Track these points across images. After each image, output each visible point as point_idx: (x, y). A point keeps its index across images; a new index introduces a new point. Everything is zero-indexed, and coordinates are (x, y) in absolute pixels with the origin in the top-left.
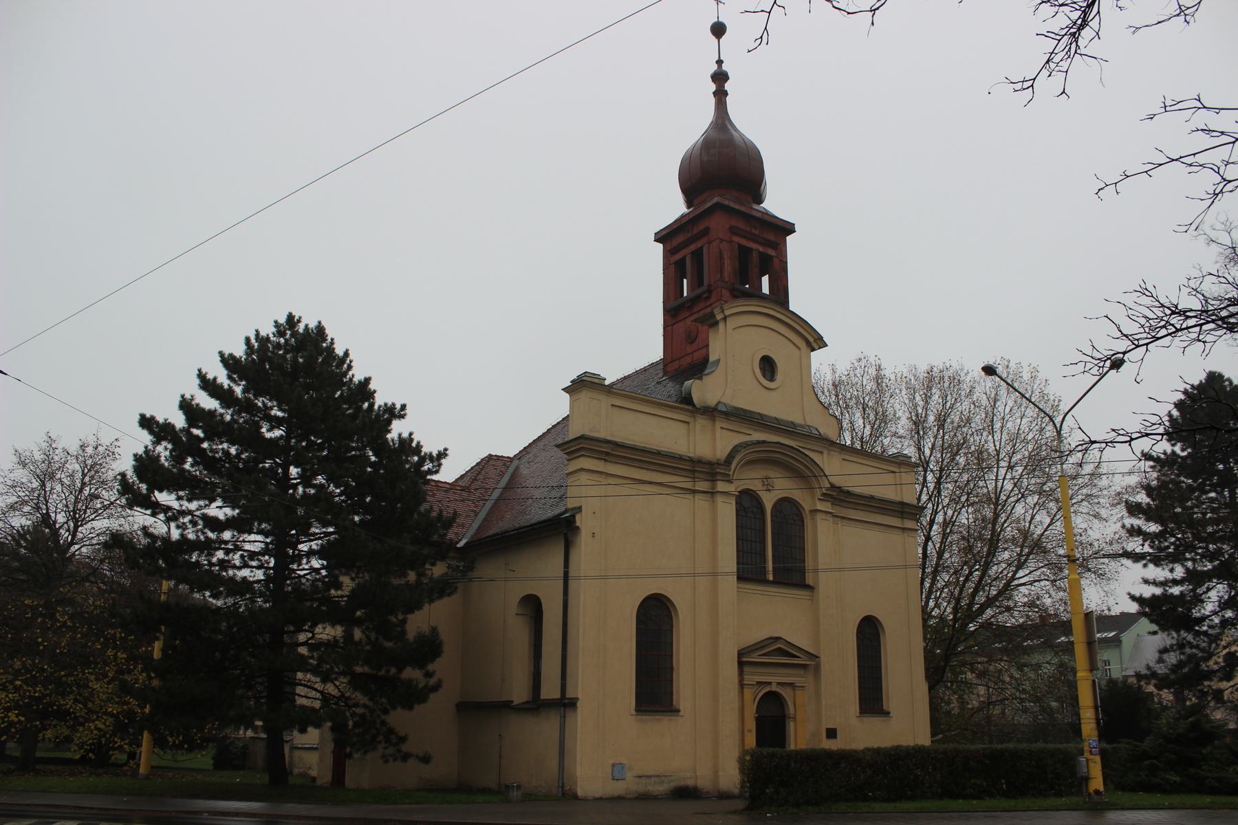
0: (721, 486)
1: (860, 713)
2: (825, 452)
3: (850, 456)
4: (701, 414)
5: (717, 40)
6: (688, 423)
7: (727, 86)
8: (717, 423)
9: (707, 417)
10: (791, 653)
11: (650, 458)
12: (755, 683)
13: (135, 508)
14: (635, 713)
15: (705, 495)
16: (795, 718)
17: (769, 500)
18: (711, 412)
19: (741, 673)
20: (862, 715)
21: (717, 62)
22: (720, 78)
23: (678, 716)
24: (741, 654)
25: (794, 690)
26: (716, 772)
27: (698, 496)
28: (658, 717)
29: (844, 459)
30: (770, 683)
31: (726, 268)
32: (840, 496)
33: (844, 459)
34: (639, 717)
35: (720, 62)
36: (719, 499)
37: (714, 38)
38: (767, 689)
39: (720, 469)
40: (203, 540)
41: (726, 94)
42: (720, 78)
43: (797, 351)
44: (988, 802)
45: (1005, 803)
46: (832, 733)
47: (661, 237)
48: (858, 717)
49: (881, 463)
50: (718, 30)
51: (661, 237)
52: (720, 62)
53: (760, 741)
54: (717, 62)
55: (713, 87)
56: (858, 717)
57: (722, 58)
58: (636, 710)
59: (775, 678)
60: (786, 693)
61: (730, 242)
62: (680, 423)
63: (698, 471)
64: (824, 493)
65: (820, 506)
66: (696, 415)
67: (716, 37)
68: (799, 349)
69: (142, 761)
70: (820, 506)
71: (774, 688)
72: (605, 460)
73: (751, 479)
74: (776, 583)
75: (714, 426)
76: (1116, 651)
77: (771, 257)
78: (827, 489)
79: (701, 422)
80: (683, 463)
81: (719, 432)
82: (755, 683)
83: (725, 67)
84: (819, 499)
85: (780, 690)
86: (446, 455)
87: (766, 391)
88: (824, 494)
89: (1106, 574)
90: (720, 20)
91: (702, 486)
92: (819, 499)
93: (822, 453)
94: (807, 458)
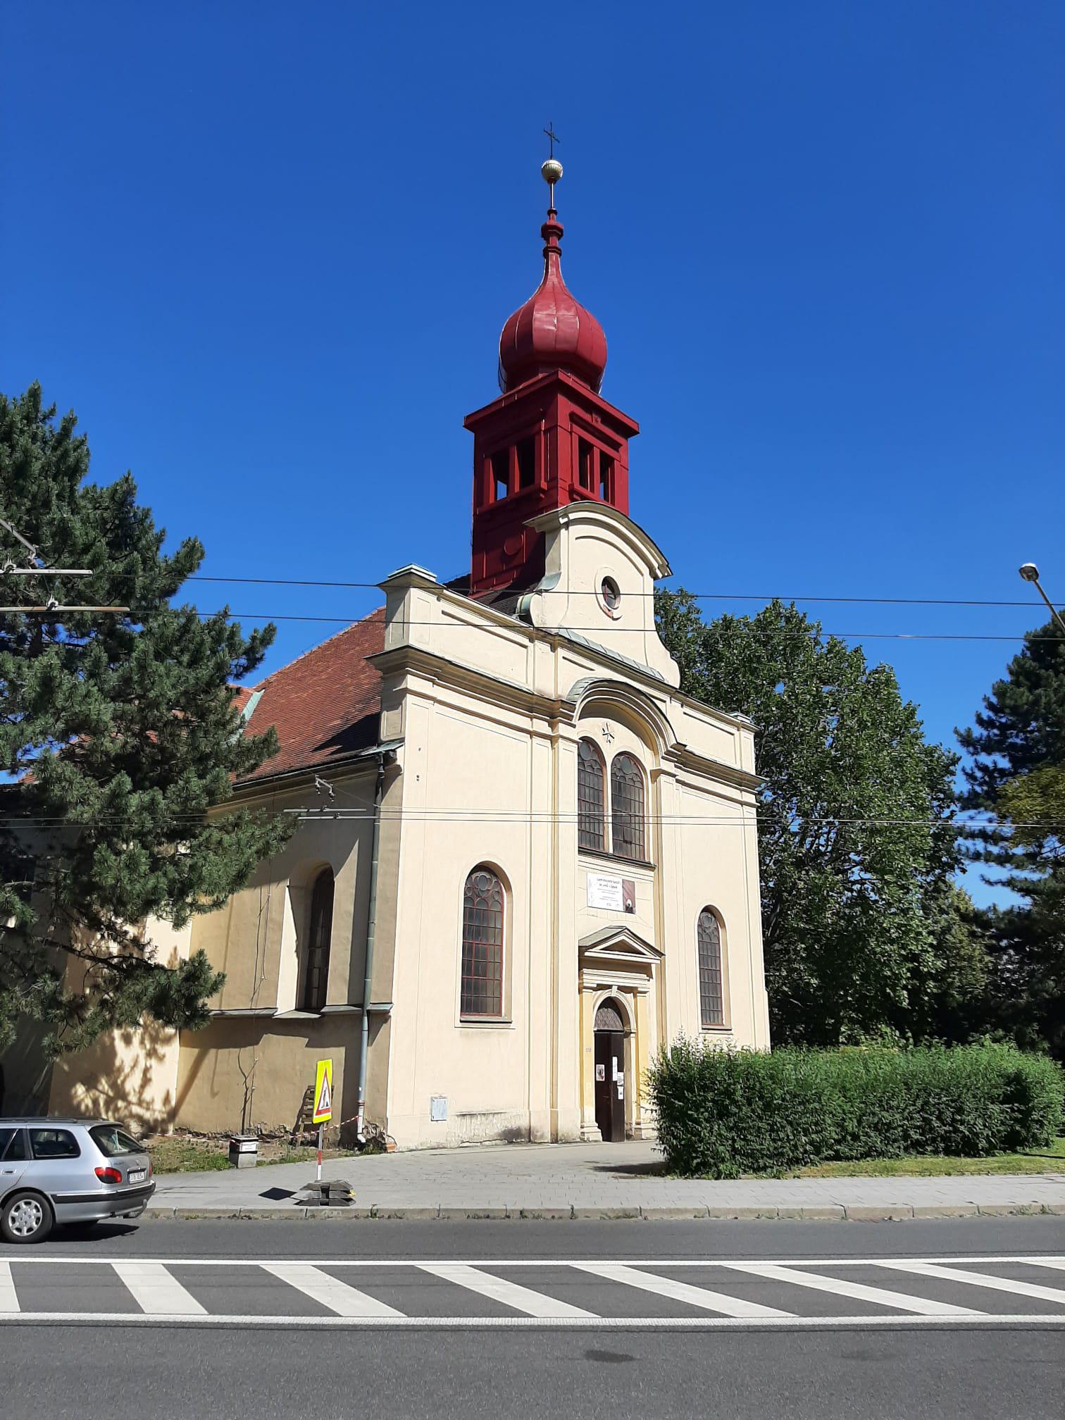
0: (563, 729)
12: (595, 986)
13: (621, 1097)
16: (636, 1033)
17: (609, 755)
18: (554, 640)
19: (580, 975)
24: (582, 950)
25: (635, 996)
26: (554, 1116)
29: (685, 713)
30: (610, 987)
32: (684, 758)
33: (685, 713)
40: (1018, 1148)
44: (929, 1160)
45: (941, 1159)
47: (472, 423)
51: (472, 423)
60: (627, 1000)
71: (614, 993)
72: (434, 683)
73: (593, 727)
79: (542, 647)
82: (595, 986)
86: (274, 630)
88: (668, 753)
89: (83, 778)
91: (542, 726)
92: (663, 758)
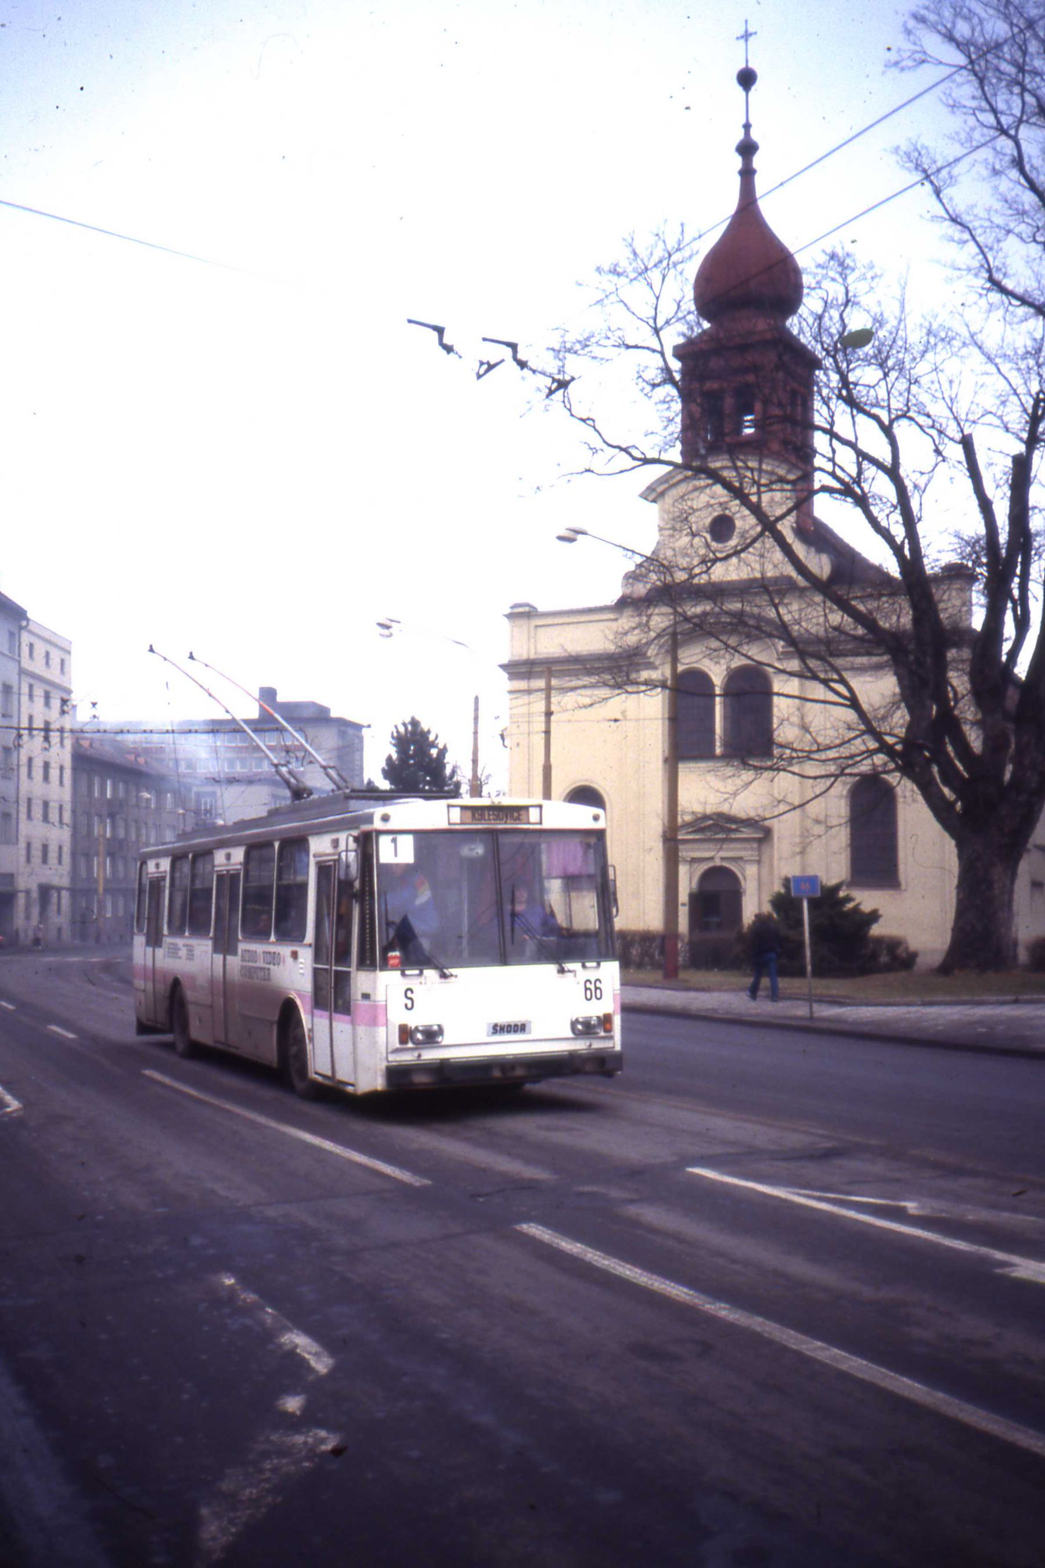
5: (744, 93)
7: (757, 161)
17: (717, 675)
22: (747, 149)
35: (747, 127)
42: (747, 149)
50: (747, 79)
52: (747, 127)
55: (738, 162)
83: (754, 135)
85: (726, 864)
90: (750, 65)
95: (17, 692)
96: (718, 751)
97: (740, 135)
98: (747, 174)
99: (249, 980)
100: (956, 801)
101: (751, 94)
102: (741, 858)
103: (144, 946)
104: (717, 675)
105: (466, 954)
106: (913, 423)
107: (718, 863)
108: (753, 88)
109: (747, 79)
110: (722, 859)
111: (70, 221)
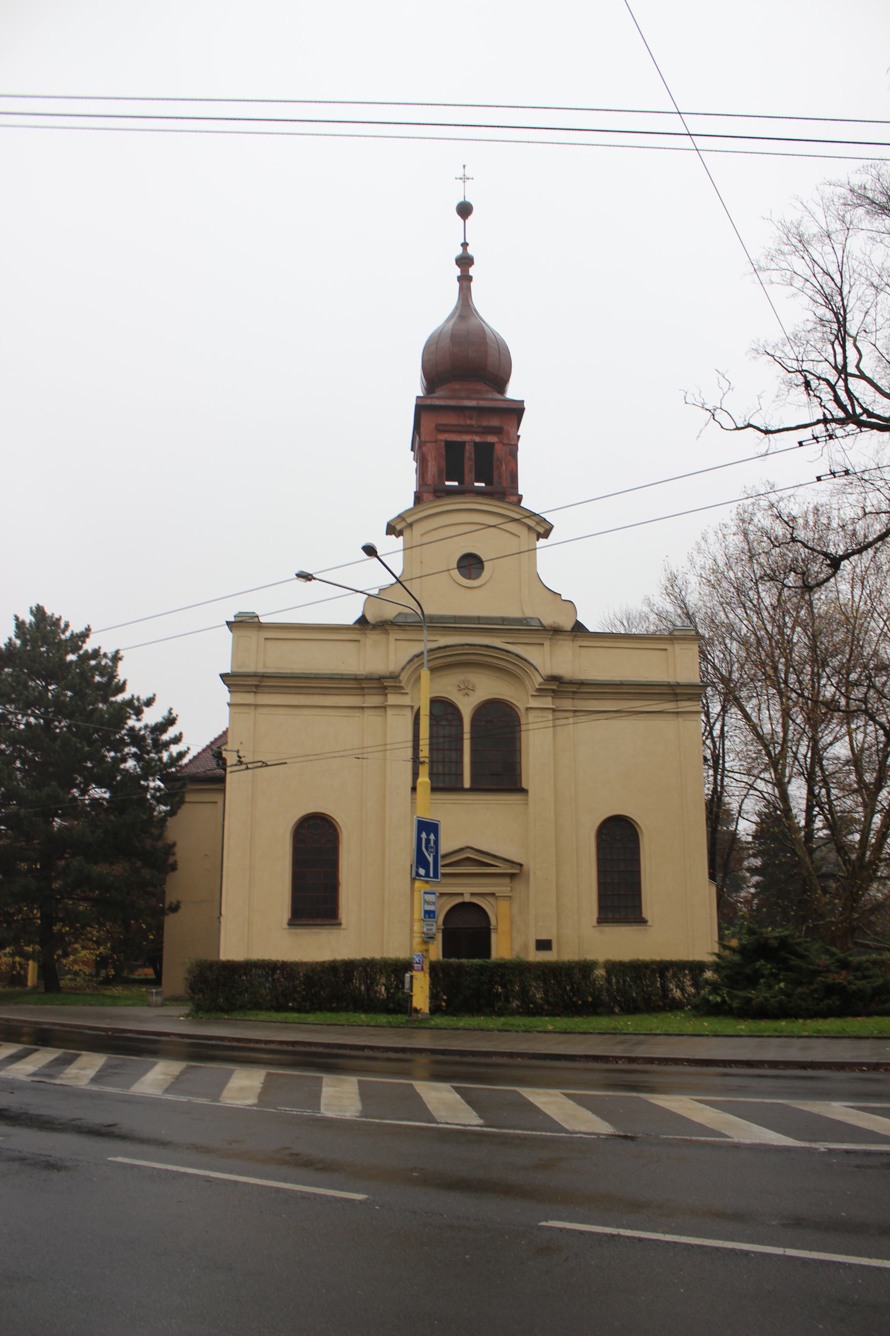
0: (392, 699)
1: (598, 922)
2: (547, 644)
3: (590, 641)
4: (371, 630)
5: (462, 221)
6: (358, 641)
7: (472, 271)
8: (391, 635)
9: (381, 632)
10: (483, 862)
11: (338, 684)
14: (287, 927)
15: (378, 710)
17: (467, 707)
20: (601, 925)
21: (462, 245)
22: (465, 262)
23: (340, 929)
27: (367, 712)
28: (316, 930)
30: (462, 894)
31: (429, 470)
33: (580, 646)
34: (293, 931)
35: (465, 245)
36: (390, 712)
37: (460, 218)
38: (459, 900)
39: (387, 682)
41: (470, 279)
42: (465, 262)
43: (516, 539)
46: (544, 945)
48: (594, 927)
49: (660, 643)
50: (464, 210)
52: (465, 245)
53: (447, 951)
54: (462, 245)
55: (457, 271)
56: (594, 927)
57: (467, 241)
58: (289, 924)
59: (467, 890)
61: (436, 442)
62: (349, 643)
63: (366, 688)
64: (538, 689)
65: (533, 703)
66: (366, 632)
67: (462, 217)
68: (519, 537)
69: (55, 1006)
70: (533, 703)
74: (472, 790)
75: (388, 640)
76: (221, 796)
77: (492, 445)
78: (540, 684)
80: (336, 682)
81: (392, 644)
83: (470, 251)
84: (532, 696)
85: (475, 900)
87: (468, 591)
88: (538, 690)
90: (467, 200)
91: (374, 700)
92: (532, 696)
93: (543, 644)
94: (511, 655)
95: (259, 702)
96: (467, 784)
97: (459, 251)
98: (465, 280)
99: (818, 968)
100: (728, 828)
101: (467, 221)
102: (493, 894)
103: (647, 928)
104: (467, 707)
105: (576, 971)
106: (763, 428)
107: (467, 899)
108: (470, 218)
109: (464, 210)
110: (472, 894)
111: (839, 157)
